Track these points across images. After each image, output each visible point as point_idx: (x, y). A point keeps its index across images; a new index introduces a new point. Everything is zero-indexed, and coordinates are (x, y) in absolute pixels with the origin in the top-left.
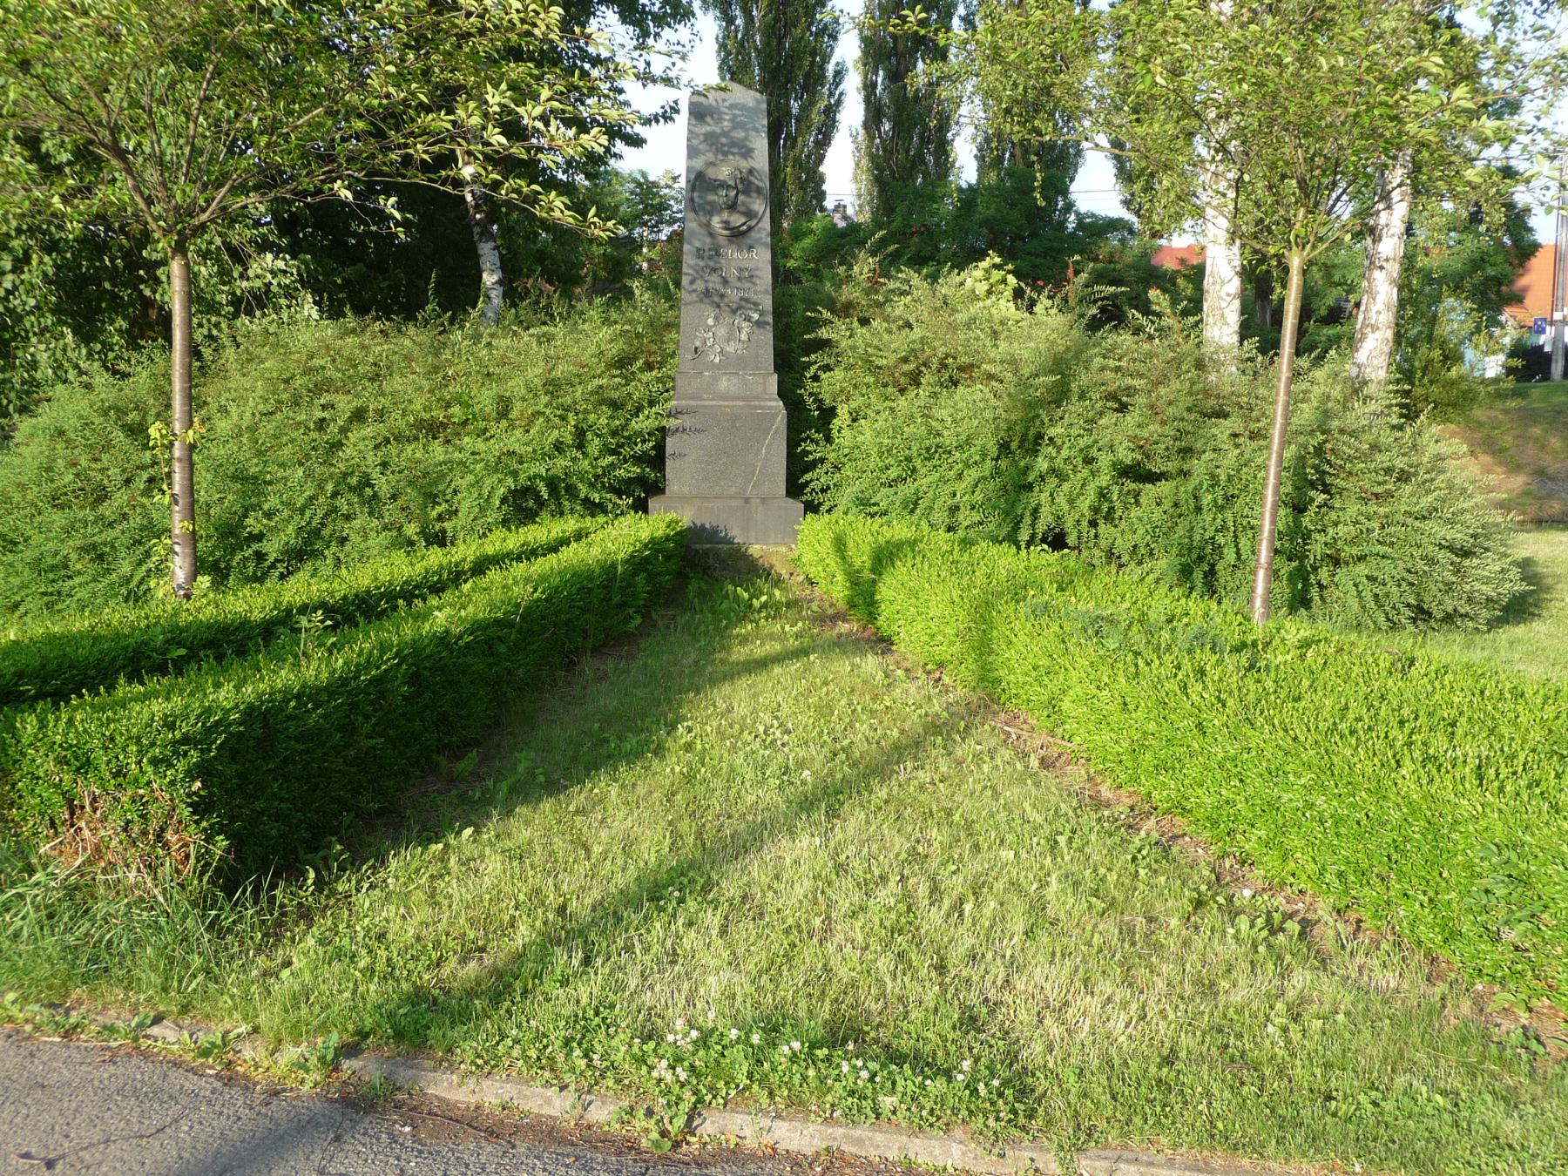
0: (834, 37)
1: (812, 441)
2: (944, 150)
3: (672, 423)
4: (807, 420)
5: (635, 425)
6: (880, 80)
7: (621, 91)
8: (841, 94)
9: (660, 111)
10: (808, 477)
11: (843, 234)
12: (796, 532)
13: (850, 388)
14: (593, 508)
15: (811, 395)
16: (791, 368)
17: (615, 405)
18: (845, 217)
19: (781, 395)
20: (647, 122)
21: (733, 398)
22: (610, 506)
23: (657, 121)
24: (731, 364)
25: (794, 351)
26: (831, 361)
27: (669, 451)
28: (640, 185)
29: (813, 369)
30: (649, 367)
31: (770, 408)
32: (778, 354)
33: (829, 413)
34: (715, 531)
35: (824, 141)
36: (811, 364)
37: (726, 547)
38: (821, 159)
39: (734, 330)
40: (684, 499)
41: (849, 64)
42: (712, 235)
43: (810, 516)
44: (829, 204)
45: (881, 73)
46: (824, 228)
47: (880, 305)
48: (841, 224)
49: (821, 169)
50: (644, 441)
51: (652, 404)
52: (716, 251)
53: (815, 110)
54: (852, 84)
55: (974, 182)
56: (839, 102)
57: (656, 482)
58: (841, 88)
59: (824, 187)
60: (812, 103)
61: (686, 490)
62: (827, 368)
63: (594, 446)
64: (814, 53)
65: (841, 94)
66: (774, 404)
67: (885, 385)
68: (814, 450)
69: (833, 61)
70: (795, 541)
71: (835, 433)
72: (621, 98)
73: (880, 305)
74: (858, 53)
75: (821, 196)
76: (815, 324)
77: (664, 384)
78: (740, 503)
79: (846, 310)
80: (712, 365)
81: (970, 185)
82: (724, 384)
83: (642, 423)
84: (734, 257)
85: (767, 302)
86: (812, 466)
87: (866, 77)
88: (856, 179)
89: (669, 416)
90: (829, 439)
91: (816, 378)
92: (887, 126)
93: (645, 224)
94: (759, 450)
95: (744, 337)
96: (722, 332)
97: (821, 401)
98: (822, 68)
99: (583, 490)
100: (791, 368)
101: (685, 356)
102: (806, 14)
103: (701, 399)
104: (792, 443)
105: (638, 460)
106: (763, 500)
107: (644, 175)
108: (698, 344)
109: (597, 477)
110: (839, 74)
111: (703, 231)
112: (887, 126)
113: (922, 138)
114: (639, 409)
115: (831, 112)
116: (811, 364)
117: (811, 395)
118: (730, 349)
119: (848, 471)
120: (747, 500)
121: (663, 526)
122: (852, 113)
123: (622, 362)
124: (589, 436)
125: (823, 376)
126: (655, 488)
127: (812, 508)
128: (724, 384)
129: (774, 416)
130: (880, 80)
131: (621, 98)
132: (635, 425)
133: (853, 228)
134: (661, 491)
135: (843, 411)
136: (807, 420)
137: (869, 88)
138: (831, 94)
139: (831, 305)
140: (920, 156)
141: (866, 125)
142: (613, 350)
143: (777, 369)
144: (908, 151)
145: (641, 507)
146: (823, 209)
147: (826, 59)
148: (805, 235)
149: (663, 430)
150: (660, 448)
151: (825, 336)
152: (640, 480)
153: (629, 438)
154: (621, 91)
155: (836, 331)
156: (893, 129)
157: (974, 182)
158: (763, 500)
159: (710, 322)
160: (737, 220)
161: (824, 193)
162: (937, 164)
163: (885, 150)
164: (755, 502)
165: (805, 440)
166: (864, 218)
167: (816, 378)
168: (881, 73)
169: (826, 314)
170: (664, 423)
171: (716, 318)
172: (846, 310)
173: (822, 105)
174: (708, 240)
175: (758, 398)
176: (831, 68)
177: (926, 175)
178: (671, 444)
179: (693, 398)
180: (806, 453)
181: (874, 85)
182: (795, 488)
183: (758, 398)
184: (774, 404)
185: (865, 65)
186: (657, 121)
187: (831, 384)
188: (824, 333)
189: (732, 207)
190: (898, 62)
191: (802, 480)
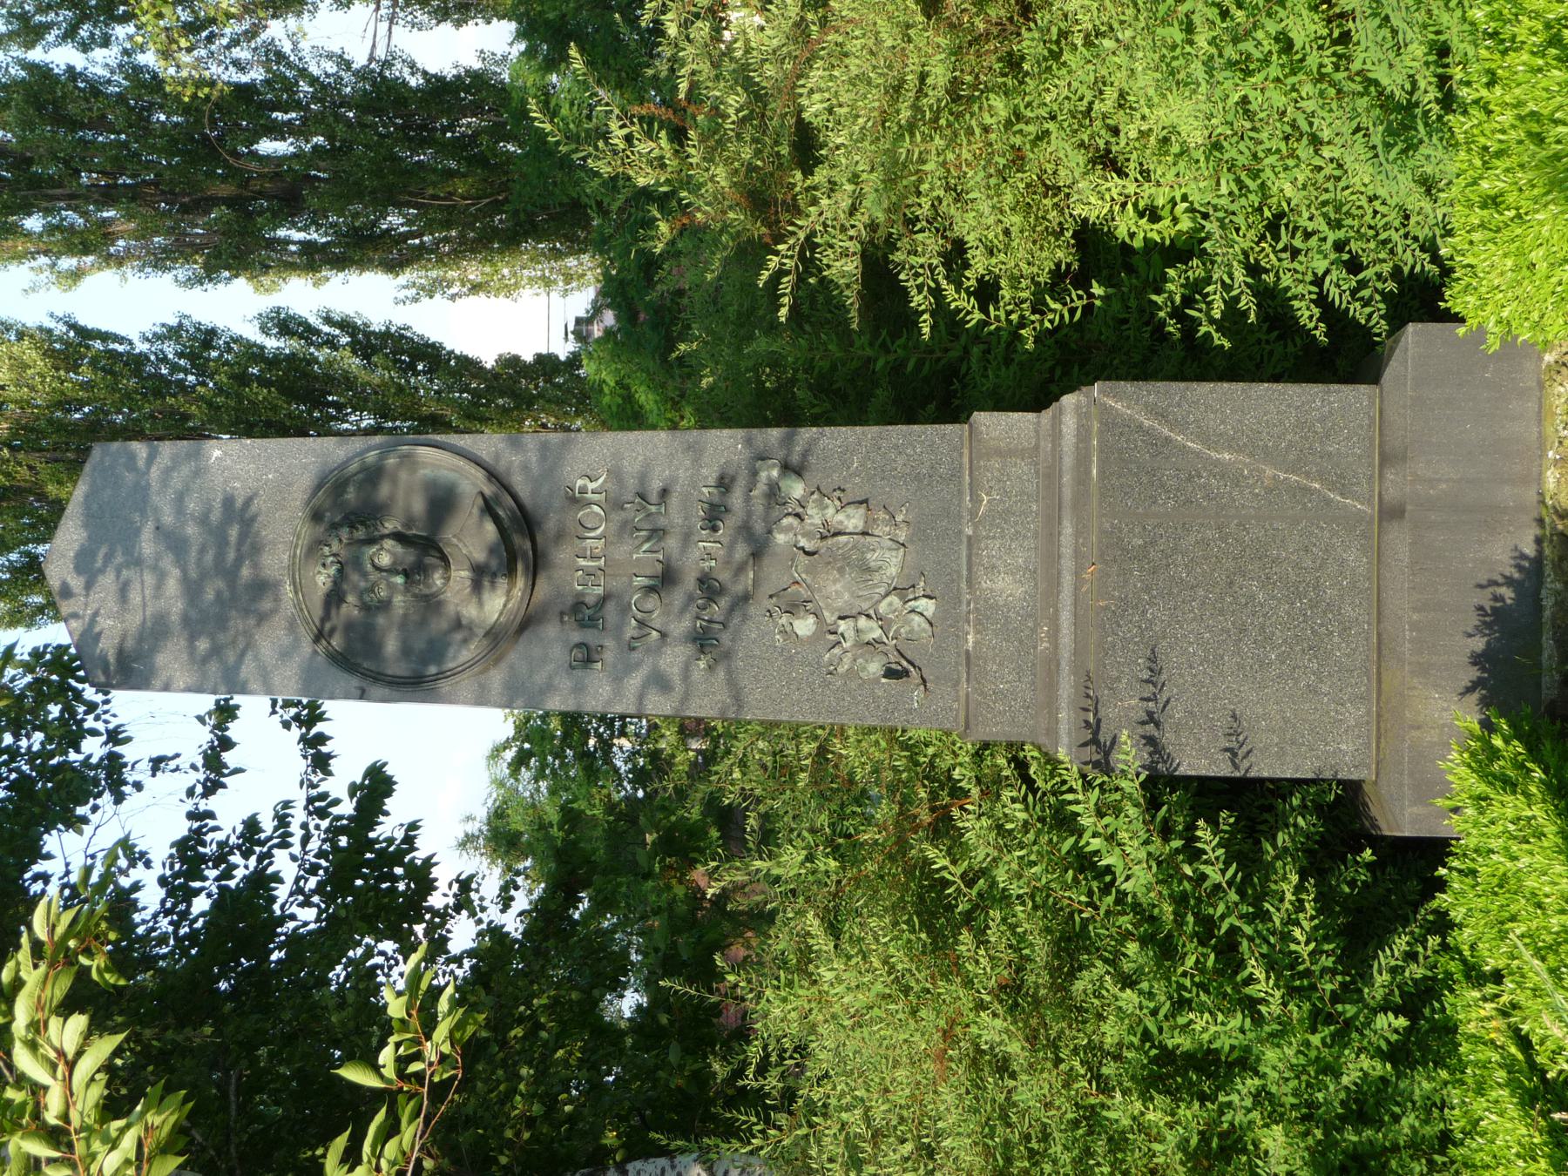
0: (209, 336)
1: (1188, 301)
2: (441, 91)
3: (1130, 756)
4: (1123, 318)
5: (1139, 880)
6: (297, 236)
7: (252, 825)
8: (328, 320)
9: (296, 732)
10: (1306, 313)
11: (628, 313)
12: (1509, 344)
13: (1019, 180)
14: (1427, 1039)
15: (1039, 307)
16: (952, 373)
17: (1072, 945)
18: (596, 310)
19: (1039, 399)
20: (321, 763)
21: (1051, 558)
22: (1417, 971)
23: (322, 739)
24: (942, 568)
25: (898, 360)
26: (930, 245)
27: (1223, 769)
28: (521, 760)
29: (958, 300)
30: (943, 828)
31: (1083, 435)
32: (907, 411)
33: (1095, 248)
34: (1495, 618)
35: (431, 355)
36: (940, 307)
37: (1552, 584)
38: (468, 365)
39: (827, 548)
40: (1385, 719)
41: (265, 302)
42: (527, 623)
43: (1456, 299)
44: (563, 349)
45: (281, 233)
46: (615, 356)
47: (758, 97)
48: (609, 318)
49: (489, 362)
50: (1194, 855)
51: (1065, 822)
52: (584, 613)
53: (364, 376)
54: (304, 296)
55: (513, 26)
56: (345, 325)
57: (1319, 809)
58: (314, 321)
59: (528, 357)
60: (348, 381)
61: (1354, 714)
62: (956, 256)
63: (1216, 1029)
64: (242, 379)
65: (328, 320)
66: (1069, 424)
67: (1013, 63)
68: (1227, 283)
69: (259, 338)
70: (1532, 351)
71: (1162, 231)
72: (268, 825)
73: (758, 97)
74: (241, 283)
75: (546, 363)
76: (817, 298)
77: (999, 781)
78: (1399, 539)
79: (765, 200)
80: (945, 625)
81: (520, 35)
82: (1005, 585)
83: (1133, 859)
84: (589, 557)
85: (726, 445)
86: (1273, 301)
87: (292, 267)
88: (508, 290)
89: (1105, 767)
90: (1183, 250)
91: (986, 292)
92: (394, 220)
93: (605, 746)
94: (1223, 471)
95: (853, 520)
96: (836, 590)
97: (1058, 274)
98: (274, 361)
99: (1359, 1067)
100: (952, 373)
101: (923, 713)
102: (158, 394)
103: (1052, 661)
104: (1195, 361)
105: (1246, 856)
106: (1385, 460)
107: (497, 752)
108: (875, 667)
109: (1317, 1018)
110: (285, 324)
111: (515, 656)
112: (394, 220)
113: (422, 144)
114: (1084, 862)
115: (367, 342)
116: (940, 307)
117: (1039, 307)
118: (891, 564)
119: (1286, 188)
120: (1391, 513)
121: (1509, 806)
122: (370, 297)
123: (936, 914)
124: (1180, 1042)
125: (979, 264)
126: (1342, 812)
127: (1421, 298)
128: (1005, 585)
129: (1110, 423)
130: (297, 236)
131: (268, 825)
132: (1139, 880)
133: (614, 293)
134: (1353, 789)
135: (1094, 199)
136: (1123, 318)
137: (313, 260)
138: (331, 343)
139: (751, 253)
140: (461, 146)
141: (393, 267)
142: (885, 937)
143: (953, 410)
144: (449, 174)
145: (1421, 860)
146: (574, 361)
147: (254, 353)
148: (629, 398)
149: (1158, 785)
150: (1209, 795)
151: (852, 266)
152: (1318, 861)
153: (1180, 901)
154: (252, 825)
155: (836, 214)
156: (399, 205)
157: (513, 26)
158: (1385, 460)
159: (804, 626)
160: (471, 538)
161: (541, 359)
162: (476, 109)
163: (448, 225)
164: (1396, 485)
165: (1189, 326)
166: (587, 265)
167: (986, 292)
168: (281, 233)
169: (784, 257)
170: (1130, 786)
171: (794, 608)
172: (765, 200)
173: (354, 363)
174: (551, 630)
175: (1051, 476)
176: (272, 343)
177: (498, 132)
178: (1198, 759)
179: (1051, 686)
180: (1233, 312)
181: (307, 247)
182: (1347, 355)
183: (1051, 476)
184: (1069, 424)
185: (266, 268)
186: (322, 739)
187: (1006, 246)
188: (844, 268)
189: (425, 548)
190: (261, 194)
191: (1320, 333)
